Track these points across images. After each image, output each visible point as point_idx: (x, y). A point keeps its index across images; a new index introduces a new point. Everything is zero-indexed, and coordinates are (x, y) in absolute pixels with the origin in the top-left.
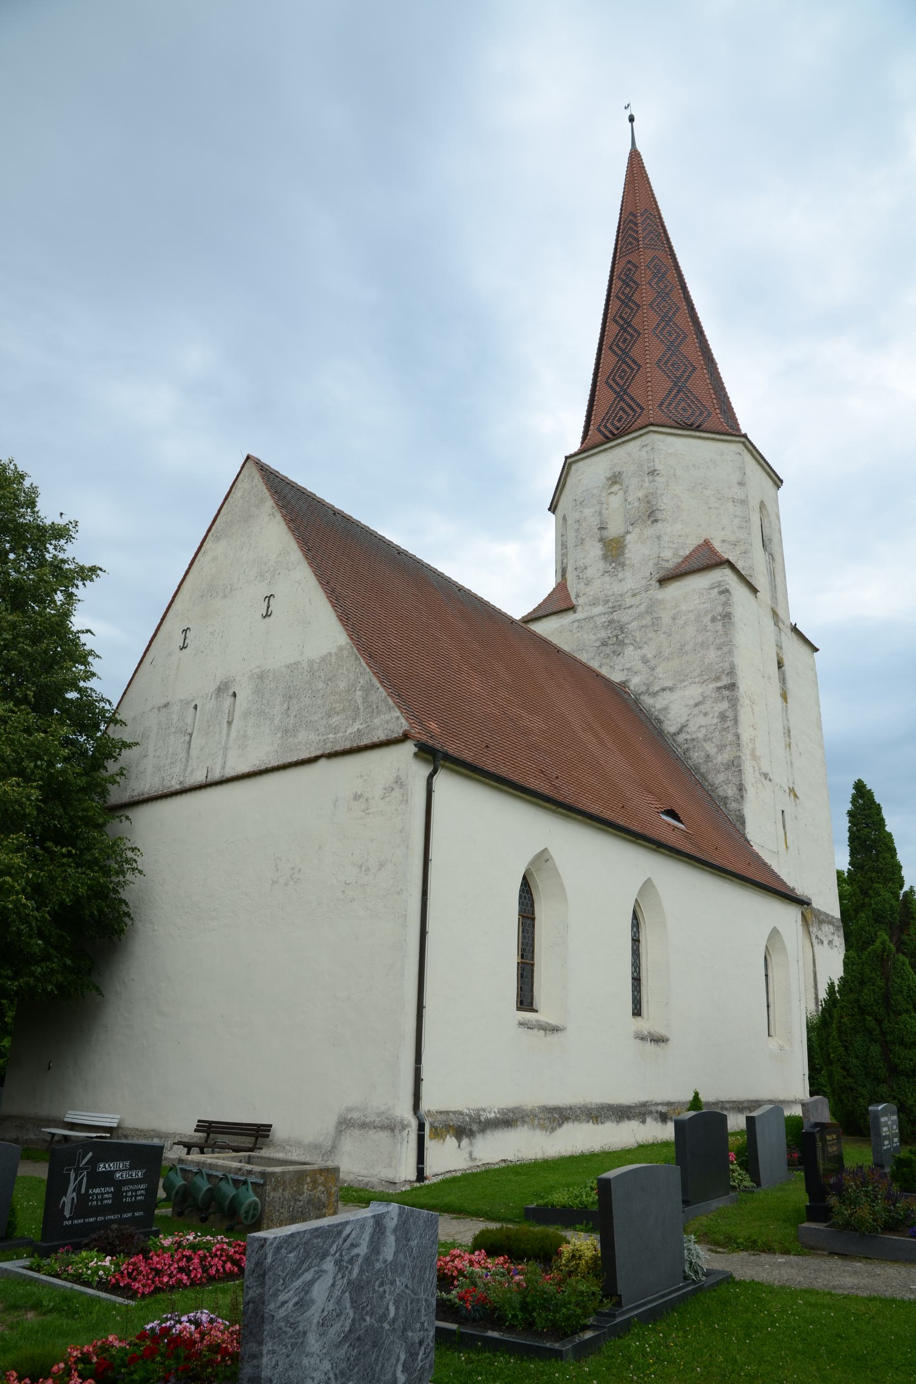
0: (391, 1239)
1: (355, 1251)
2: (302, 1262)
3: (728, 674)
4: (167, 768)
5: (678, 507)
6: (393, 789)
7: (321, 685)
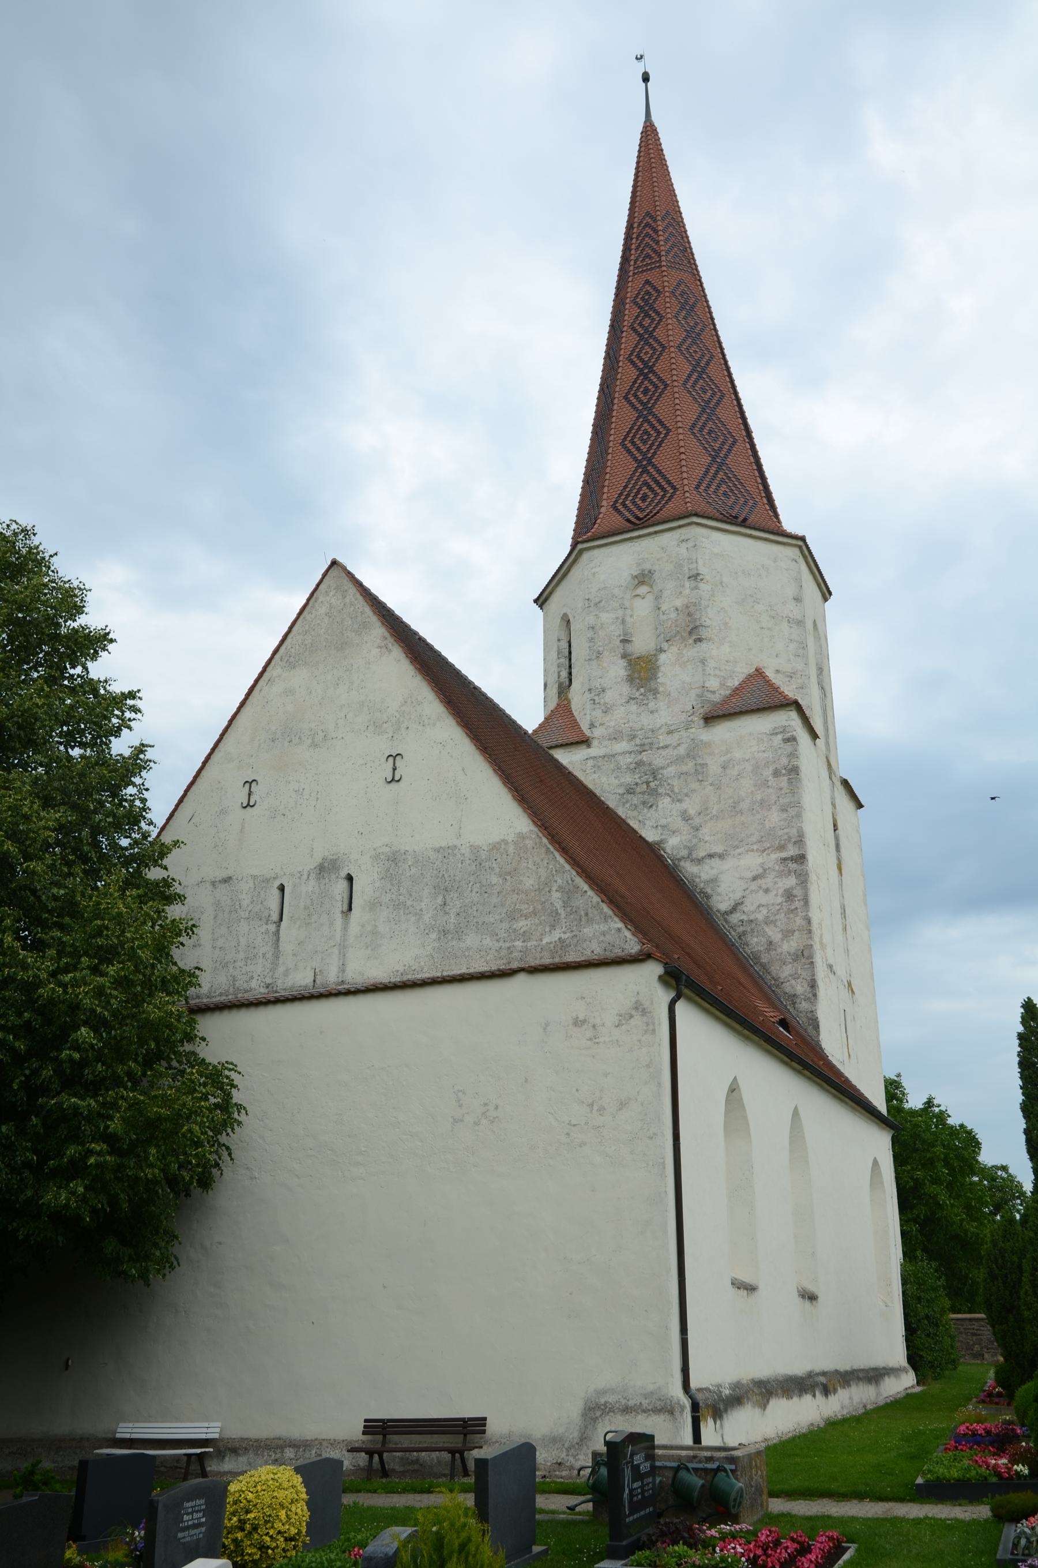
4: (239, 964)
5: (726, 624)
6: (632, 1016)
7: (494, 880)
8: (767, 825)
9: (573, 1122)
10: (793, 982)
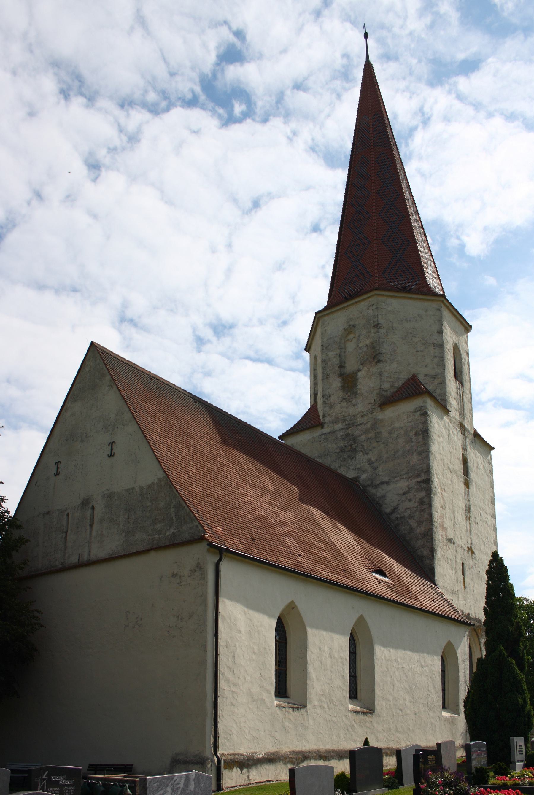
0: (192, 783)
1: (179, 786)
2: (159, 787)
3: (425, 472)
6: (195, 571)
7: (148, 504)
8: (411, 463)
9: (171, 626)
10: (422, 549)
